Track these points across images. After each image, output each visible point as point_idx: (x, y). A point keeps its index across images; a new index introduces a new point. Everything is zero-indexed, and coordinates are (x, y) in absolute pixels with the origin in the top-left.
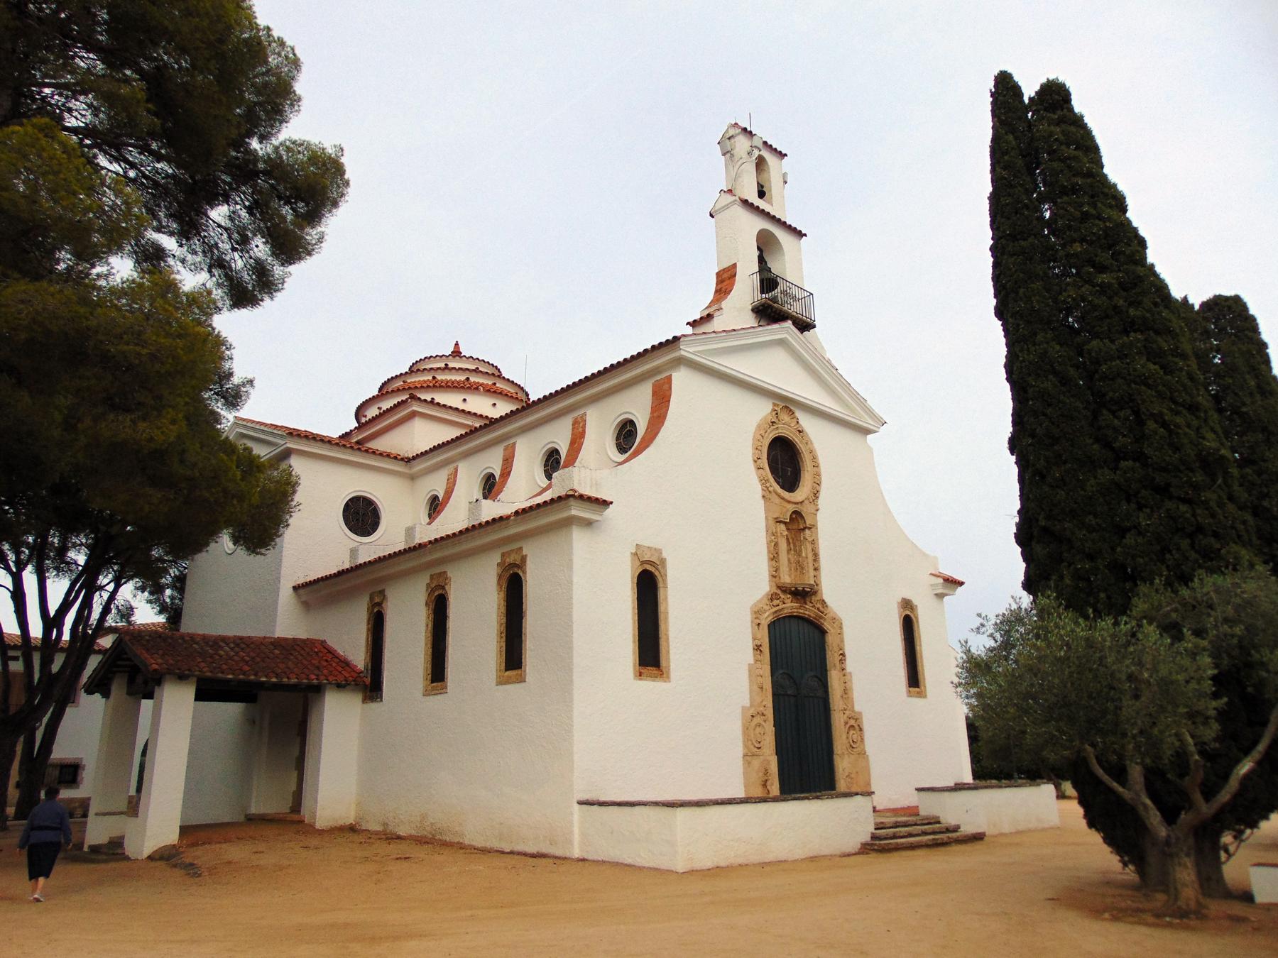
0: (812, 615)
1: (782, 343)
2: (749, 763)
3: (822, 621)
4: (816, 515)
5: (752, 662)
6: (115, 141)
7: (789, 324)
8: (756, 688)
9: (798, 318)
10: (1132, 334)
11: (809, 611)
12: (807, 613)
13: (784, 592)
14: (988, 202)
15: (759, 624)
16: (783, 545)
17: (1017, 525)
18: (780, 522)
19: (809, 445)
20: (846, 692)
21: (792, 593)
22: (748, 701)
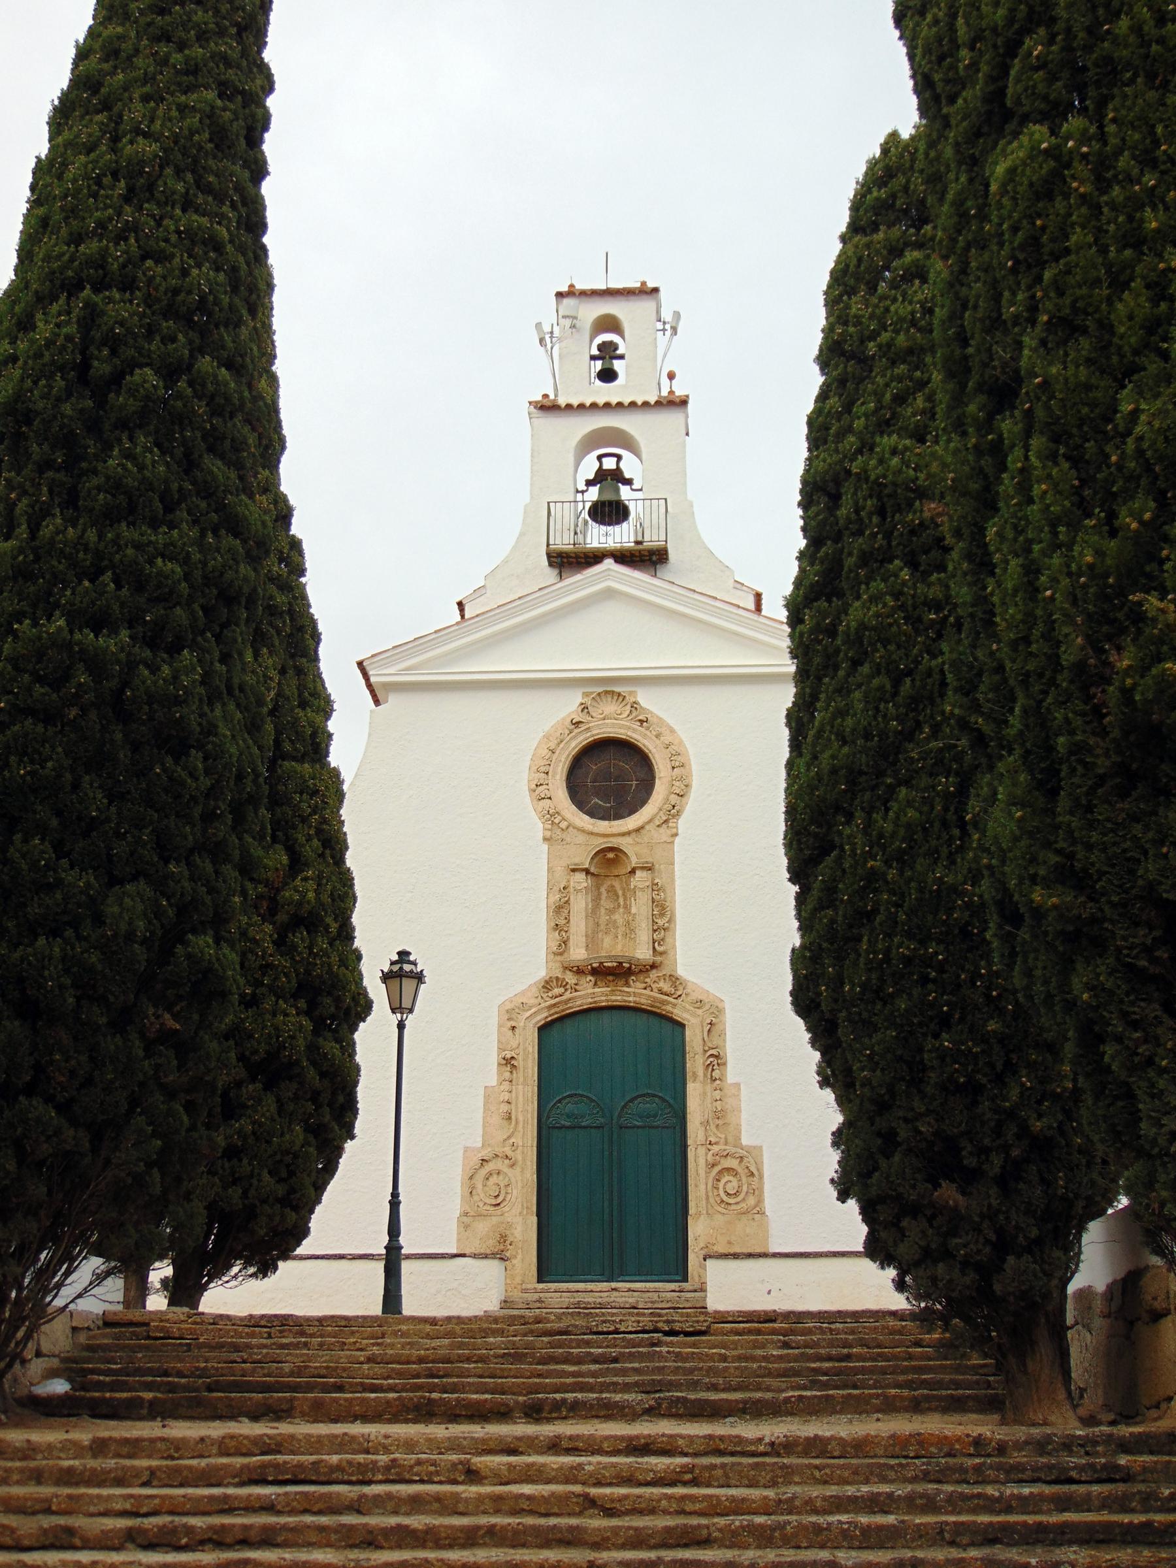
0: (643, 1001)
1: (609, 594)
2: (467, 1227)
3: (669, 1008)
4: (672, 842)
5: (494, 1083)
6: (1155, 310)
7: (609, 563)
8: (496, 1120)
9: (617, 550)
10: (137, 371)
11: (635, 993)
12: (631, 999)
13: (579, 971)
14: (47, 128)
15: (513, 1028)
16: (579, 905)
17: (839, 1138)
18: (573, 870)
19: (667, 738)
20: (720, 1117)
21: (595, 972)
22: (480, 1139)
